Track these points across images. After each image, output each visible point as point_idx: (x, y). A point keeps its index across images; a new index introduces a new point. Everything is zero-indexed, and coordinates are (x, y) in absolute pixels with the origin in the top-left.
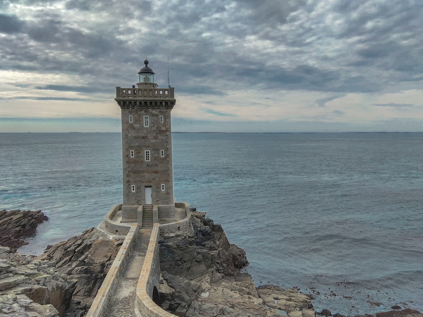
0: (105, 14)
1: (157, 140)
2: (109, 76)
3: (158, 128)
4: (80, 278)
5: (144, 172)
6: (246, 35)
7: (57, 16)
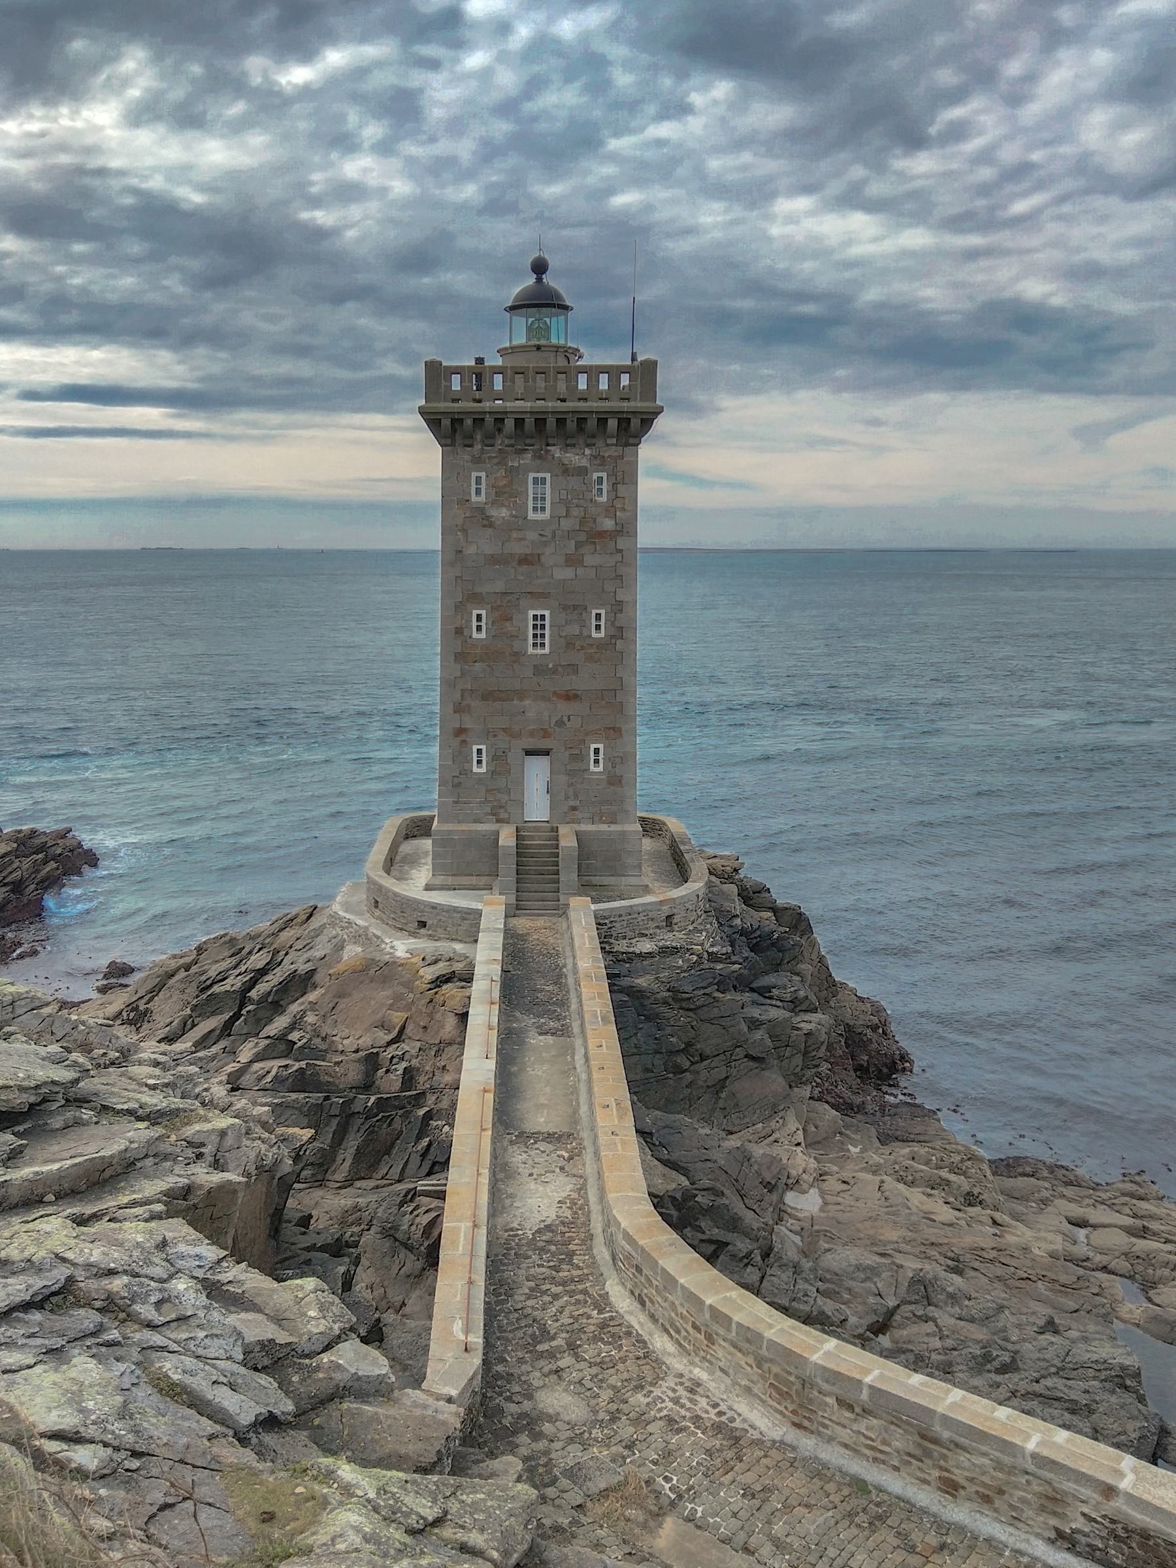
0: (257, 139)
1: (580, 571)
2: (280, 349)
3: (583, 521)
4: (279, 1110)
5: (521, 694)
6: (773, 195)
7: (91, 150)
